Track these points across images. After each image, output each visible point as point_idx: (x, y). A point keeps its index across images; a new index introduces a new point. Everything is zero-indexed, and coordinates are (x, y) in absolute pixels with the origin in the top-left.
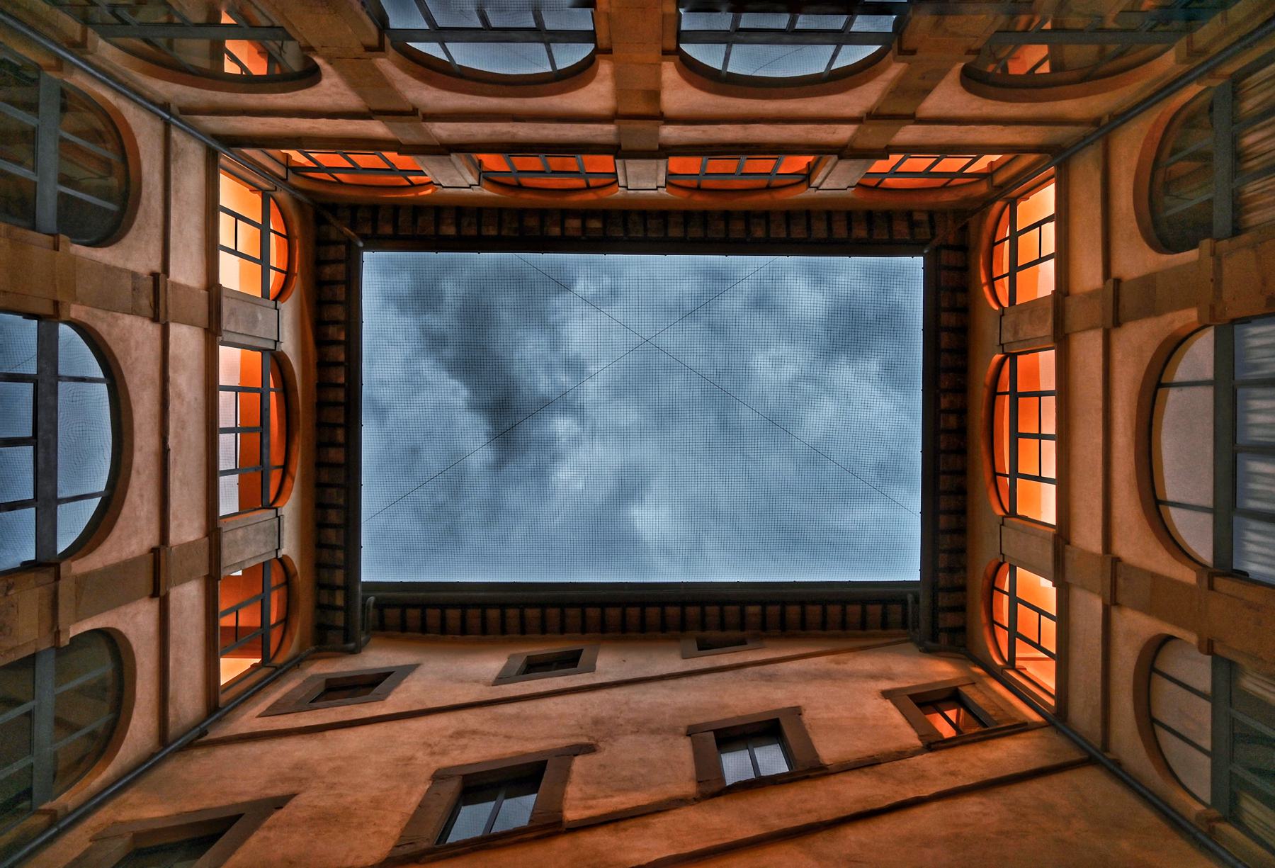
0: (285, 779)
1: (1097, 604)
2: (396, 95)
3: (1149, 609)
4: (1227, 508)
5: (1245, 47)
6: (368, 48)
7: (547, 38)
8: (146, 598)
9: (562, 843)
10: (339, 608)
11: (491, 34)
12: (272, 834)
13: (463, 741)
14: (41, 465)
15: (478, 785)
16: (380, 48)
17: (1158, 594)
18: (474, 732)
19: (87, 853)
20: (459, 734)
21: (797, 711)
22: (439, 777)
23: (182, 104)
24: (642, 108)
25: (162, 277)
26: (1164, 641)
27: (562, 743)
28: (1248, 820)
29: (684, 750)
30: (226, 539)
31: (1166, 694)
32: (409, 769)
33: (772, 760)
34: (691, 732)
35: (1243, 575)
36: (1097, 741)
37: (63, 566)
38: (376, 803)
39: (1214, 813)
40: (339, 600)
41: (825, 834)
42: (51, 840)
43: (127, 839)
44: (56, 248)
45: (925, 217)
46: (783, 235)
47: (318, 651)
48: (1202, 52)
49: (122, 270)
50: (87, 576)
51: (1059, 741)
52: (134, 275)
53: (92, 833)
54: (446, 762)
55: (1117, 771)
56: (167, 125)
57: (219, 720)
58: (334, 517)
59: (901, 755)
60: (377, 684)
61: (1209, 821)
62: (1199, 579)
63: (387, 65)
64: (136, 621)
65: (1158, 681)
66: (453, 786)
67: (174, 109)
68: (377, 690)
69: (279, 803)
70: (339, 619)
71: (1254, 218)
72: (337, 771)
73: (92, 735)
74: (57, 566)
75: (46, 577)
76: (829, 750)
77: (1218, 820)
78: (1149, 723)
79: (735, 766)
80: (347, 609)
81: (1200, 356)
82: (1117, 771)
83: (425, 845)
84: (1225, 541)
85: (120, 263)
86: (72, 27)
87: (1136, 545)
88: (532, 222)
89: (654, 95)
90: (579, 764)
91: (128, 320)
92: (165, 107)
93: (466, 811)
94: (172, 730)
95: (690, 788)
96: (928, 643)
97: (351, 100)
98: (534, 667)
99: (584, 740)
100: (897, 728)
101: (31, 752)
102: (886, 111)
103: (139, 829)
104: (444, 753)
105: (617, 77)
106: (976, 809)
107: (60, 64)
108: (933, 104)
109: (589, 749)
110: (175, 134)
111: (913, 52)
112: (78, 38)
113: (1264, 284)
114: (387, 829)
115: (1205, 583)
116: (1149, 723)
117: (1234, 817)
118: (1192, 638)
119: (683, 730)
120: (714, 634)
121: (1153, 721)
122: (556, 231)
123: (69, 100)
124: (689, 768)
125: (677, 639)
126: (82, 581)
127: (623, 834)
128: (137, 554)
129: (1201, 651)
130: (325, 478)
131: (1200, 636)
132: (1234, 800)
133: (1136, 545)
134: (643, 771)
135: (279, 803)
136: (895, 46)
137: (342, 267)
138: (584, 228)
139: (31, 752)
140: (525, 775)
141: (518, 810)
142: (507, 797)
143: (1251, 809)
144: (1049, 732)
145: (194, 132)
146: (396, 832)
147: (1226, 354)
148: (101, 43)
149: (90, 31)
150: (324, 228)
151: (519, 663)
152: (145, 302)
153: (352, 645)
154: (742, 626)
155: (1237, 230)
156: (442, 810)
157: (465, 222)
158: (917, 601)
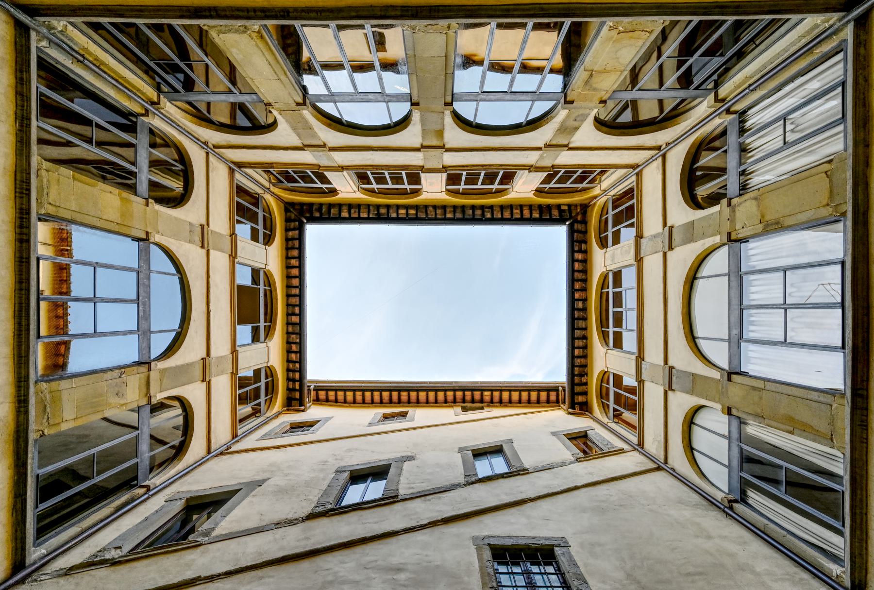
0: (264, 471)
1: (660, 390)
2: (315, 135)
3: (691, 392)
4: (737, 339)
5: (752, 91)
6: (298, 104)
7: (387, 99)
8: (199, 382)
9: (397, 507)
10: (297, 390)
11: (359, 96)
12: (254, 499)
13: (351, 454)
14: (141, 314)
15: (358, 477)
16: (304, 104)
17: (694, 384)
18: (357, 449)
19: (162, 507)
20: (349, 450)
21: (510, 441)
22: (339, 471)
23: (214, 143)
24: (435, 142)
25: (206, 227)
26: (698, 409)
27: (399, 455)
28: (750, 501)
29: (458, 459)
30: (240, 356)
31: (698, 434)
32: (325, 467)
33: (499, 465)
34: (461, 450)
35: (745, 374)
36: (662, 458)
37: (153, 364)
38: (307, 484)
39: (732, 497)
40: (297, 386)
41: (531, 504)
42: (145, 500)
43: (183, 501)
44: (147, 205)
45: (566, 208)
46: (500, 216)
47: (287, 410)
48: (723, 100)
49: (185, 221)
50: (165, 370)
51: (641, 458)
52: (191, 224)
53: (166, 497)
54: (343, 464)
55: (674, 473)
56: (207, 153)
57: (237, 441)
58: (294, 348)
59: (563, 464)
60: (312, 426)
61: (729, 502)
62: (722, 376)
63: (307, 113)
64: (194, 393)
65: (694, 427)
66: (346, 475)
67: (210, 145)
68: (313, 428)
69: (259, 483)
70: (297, 395)
71: (755, 180)
72: (289, 467)
73: (173, 447)
74: (149, 364)
75: (143, 369)
76: (528, 462)
77: (736, 501)
78: (690, 449)
79: (483, 468)
80: (301, 390)
81: (719, 262)
82: (674, 473)
83: (329, 507)
84: (735, 354)
85: (183, 217)
86: (152, 94)
87: (682, 358)
88: (383, 211)
89: (440, 133)
90: (406, 465)
91: (188, 245)
92: (206, 143)
93: (352, 488)
94: (213, 447)
95: (462, 480)
96: (570, 410)
97: (296, 141)
98: (386, 417)
99: (410, 454)
100: (566, 452)
101: (137, 456)
102: (554, 142)
103: (189, 495)
104: (342, 459)
105: (423, 121)
106: (606, 492)
107: (147, 113)
108: (578, 139)
109: (411, 458)
110: (211, 158)
111: (572, 102)
112: (155, 99)
113: (763, 216)
114: (311, 497)
115: (726, 377)
116: (690, 449)
117: (743, 500)
118: (719, 406)
119: (457, 450)
120: (469, 405)
121: (692, 449)
122: (394, 215)
123: (158, 140)
124: (460, 470)
125: (452, 407)
126: (162, 372)
127: (428, 502)
128: (194, 360)
129: (723, 412)
130: (290, 329)
131: (723, 405)
132: (743, 493)
133: (682, 358)
134: (438, 470)
135: (259, 483)
136: (562, 100)
137: (297, 232)
138: (407, 214)
139: (137, 456)
140: (379, 472)
141: (375, 489)
142: (371, 481)
143: (754, 496)
144: (635, 453)
145: (221, 158)
146: (316, 499)
147: (736, 260)
148: (168, 104)
149: (162, 96)
150: (288, 214)
151: (379, 417)
152: (197, 238)
153: (303, 408)
154: (482, 401)
155: (744, 188)
156: (339, 488)
157: (353, 211)
158: (564, 390)
